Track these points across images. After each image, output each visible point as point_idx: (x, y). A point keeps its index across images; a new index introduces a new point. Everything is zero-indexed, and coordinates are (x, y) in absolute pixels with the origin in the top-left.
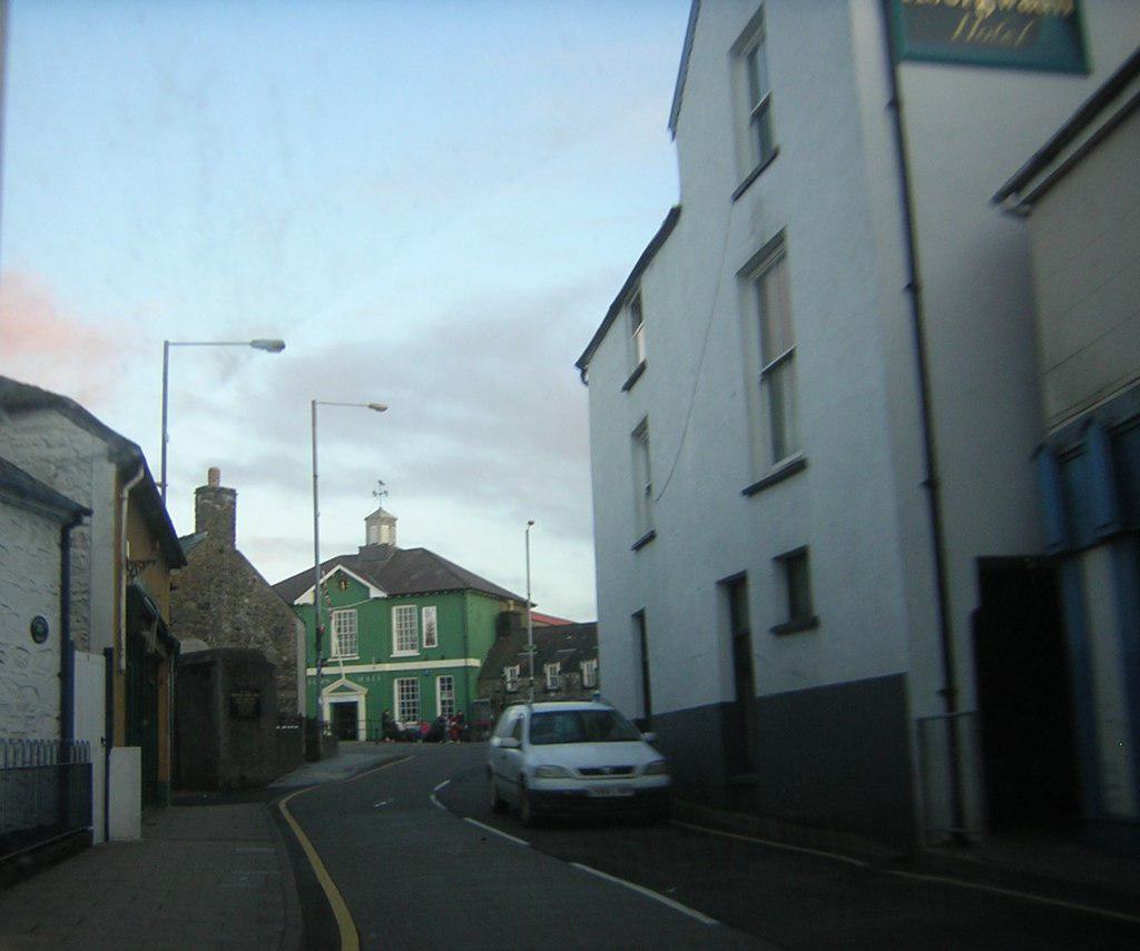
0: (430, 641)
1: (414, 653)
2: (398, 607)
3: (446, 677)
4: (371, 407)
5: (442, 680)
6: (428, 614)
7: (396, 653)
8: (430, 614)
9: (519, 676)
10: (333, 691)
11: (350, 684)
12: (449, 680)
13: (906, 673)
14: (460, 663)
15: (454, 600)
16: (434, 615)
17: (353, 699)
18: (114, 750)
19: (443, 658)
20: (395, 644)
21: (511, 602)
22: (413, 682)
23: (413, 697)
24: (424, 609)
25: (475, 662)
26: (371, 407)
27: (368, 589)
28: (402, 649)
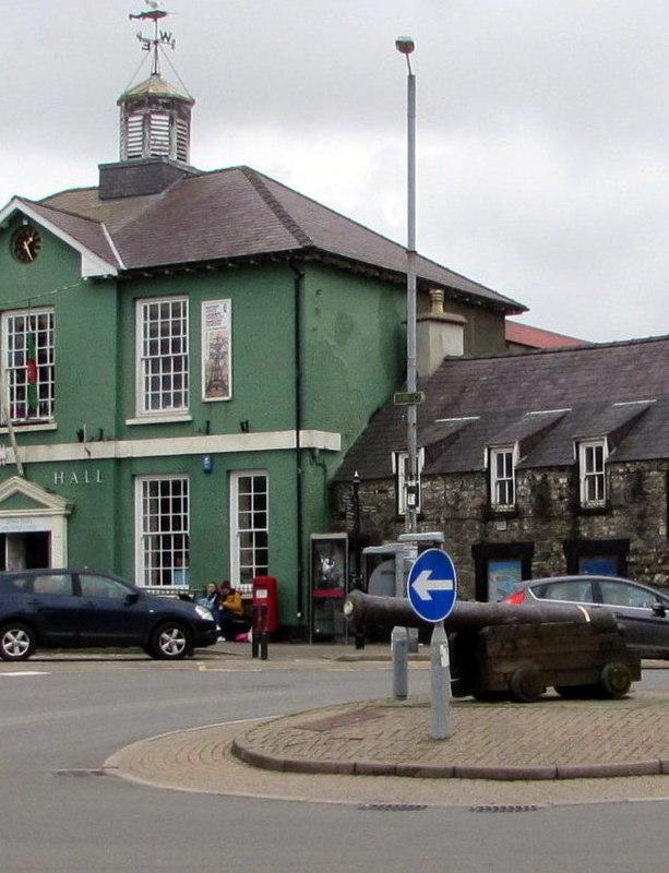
0: (216, 384)
1: (181, 413)
2: (149, 303)
3: (252, 475)
4: (411, 78)
5: (244, 484)
6: (215, 319)
7: (144, 414)
8: (217, 318)
9: (425, 477)
10: (47, 507)
11: (33, 491)
12: (260, 484)
13: (100, 166)
14: (285, 439)
15: (275, 294)
17: (38, 526)
18: (301, 432)
19: (245, 428)
20: (141, 392)
21: (438, 294)
22: (176, 485)
23: (177, 524)
24: (205, 305)
25: (332, 441)
26: (411, 78)
27: (77, 255)
28: (155, 406)
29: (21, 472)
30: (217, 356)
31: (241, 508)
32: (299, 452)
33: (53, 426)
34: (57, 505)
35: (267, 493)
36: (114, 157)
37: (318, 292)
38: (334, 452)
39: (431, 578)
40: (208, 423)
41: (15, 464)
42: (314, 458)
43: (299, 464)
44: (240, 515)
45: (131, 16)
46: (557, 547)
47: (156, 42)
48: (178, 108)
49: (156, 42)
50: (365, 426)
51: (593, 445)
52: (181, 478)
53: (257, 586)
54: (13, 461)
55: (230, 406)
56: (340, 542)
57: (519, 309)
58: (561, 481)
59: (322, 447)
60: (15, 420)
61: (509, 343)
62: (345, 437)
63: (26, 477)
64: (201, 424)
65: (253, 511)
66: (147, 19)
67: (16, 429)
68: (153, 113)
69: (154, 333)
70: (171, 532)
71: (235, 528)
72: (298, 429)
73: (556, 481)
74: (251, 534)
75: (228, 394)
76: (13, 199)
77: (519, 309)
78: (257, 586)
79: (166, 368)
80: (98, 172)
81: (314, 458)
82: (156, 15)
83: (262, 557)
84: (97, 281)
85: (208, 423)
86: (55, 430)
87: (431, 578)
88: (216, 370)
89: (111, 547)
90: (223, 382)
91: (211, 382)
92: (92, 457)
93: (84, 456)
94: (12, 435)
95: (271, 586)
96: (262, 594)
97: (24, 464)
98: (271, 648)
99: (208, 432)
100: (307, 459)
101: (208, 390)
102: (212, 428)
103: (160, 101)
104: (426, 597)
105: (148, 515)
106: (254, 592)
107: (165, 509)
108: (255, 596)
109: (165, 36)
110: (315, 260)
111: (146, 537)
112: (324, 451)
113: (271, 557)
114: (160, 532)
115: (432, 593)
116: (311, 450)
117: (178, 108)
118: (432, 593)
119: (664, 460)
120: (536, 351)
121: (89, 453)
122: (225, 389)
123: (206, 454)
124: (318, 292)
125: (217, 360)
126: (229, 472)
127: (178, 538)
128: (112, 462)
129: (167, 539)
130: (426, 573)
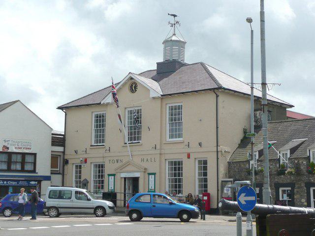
4: (252, 31)
26: (252, 31)
28: (172, 137)
36: (161, 60)
37: (223, 101)
39: (245, 196)
44: (199, 172)
46: (303, 185)
47: (175, 24)
48: (181, 44)
49: (175, 24)
51: (285, 152)
56: (231, 181)
57: (291, 106)
58: (304, 162)
60: (130, 142)
61: (288, 117)
69: (172, 115)
73: (302, 163)
77: (291, 106)
78: (204, 195)
79: (176, 126)
80: (156, 65)
82: (175, 16)
83: (206, 186)
84: (154, 98)
87: (245, 196)
95: (208, 195)
98: (207, 216)
104: (243, 203)
106: (203, 198)
107: (175, 170)
109: (177, 22)
110: (222, 91)
111: (169, 179)
115: (245, 201)
117: (181, 44)
118: (245, 201)
119: (23, 167)
120: (295, 120)
124: (223, 101)
129: (176, 179)
130: (243, 195)
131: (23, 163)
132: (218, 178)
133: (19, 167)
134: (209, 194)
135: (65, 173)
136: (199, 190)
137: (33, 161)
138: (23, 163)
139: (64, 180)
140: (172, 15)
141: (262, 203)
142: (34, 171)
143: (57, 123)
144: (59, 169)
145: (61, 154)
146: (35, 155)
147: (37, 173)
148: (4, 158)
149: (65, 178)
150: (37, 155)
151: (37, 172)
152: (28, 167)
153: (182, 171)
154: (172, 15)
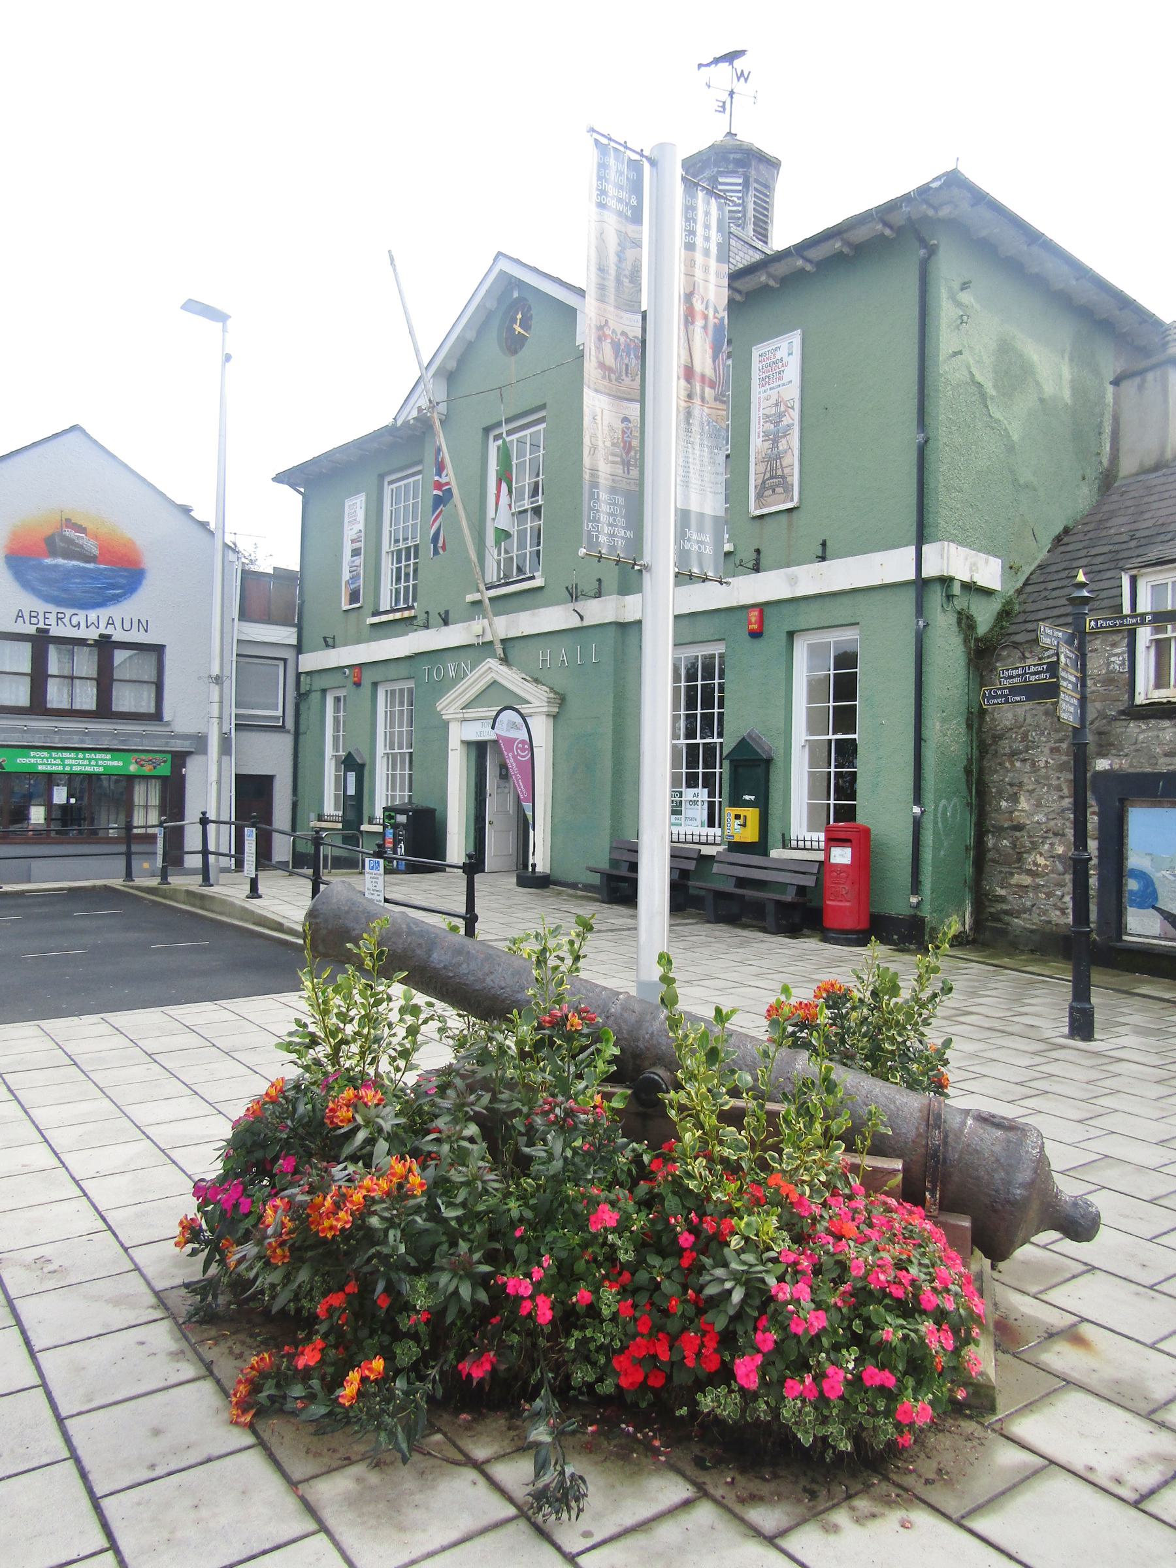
6: (775, 368)
14: (897, 565)
16: (792, 372)
18: (925, 548)
25: (988, 572)
29: (500, 652)
30: (774, 439)
31: (811, 699)
32: (921, 584)
33: (538, 582)
34: (537, 699)
35: (832, 640)
38: (987, 592)
40: (758, 551)
41: (491, 642)
42: (950, 597)
43: (920, 611)
45: (700, 66)
50: (1042, 556)
52: (717, 649)
53: (834, 840)
54: (488, 638)
55: (795, 514)
59: (967, 579)
62: (1011, 569)
63: (505, 660)
64: (748, 556)
65: (831, 704)
66: (721, 65)
67: (493, 593)
68: (721, 174)
70: (698, 741)
71: (800, 734)
72: (921, 540)
74: (830, 741)
75: (792, 500)
76: (495, 260)
78: (834, 840)
81: (950, 597)
85: (758, 551)
86: (540, 588)
88: (774, 459)
89: (608, 762)
90: (783, 477)
91: (764, 482)
92: (586, 623)
93: (575, 622)
94: (487, 601)
95: (861, 841)
96: (842, 856)
97: (502, 641)
99: (757, 569)
100: (936, 597)
101: (760, 496)
102: (763, 562)
103: (732, 156)
105: (682, 712)
108: (828, 856)
112: (970, 588)
113: (861, 786)
114: (831, 737)
116: (946, 581)
121: (582, 618)
122: (788, 489)
123: (753, 606)
125: (775, 442)
126: (791, 635)
127: (710, 749)
128: (614, 628)
131: (105, 682)
132: (919, 740)
133: (86, 698)
134: (866, 832)
135: (302, 728)
136: (811, 807)
137: (154, 679)
138: (105, 682)
139: (300, 765)
140: (717, 61)
141: (29, 881)
142: (157, 716)
143: (272, 538)
144: (279, 713)
145: (289, 655)
146: (157, 650)
147: (168, 724)
148: (20, 658)
149: (300, 745)
150: (168, 651)
151: (166, 719)
152: (126, 699)
153: (721, 706)
154: (717, 61)
